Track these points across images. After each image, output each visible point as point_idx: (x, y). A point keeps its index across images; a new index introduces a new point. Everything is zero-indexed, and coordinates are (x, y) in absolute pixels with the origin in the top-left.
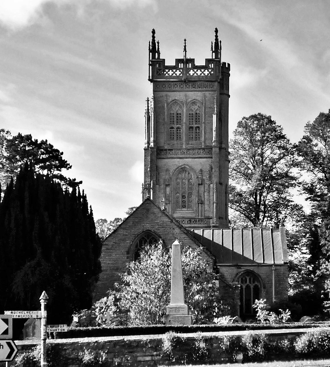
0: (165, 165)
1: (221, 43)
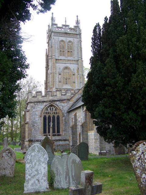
1: (78, 17)
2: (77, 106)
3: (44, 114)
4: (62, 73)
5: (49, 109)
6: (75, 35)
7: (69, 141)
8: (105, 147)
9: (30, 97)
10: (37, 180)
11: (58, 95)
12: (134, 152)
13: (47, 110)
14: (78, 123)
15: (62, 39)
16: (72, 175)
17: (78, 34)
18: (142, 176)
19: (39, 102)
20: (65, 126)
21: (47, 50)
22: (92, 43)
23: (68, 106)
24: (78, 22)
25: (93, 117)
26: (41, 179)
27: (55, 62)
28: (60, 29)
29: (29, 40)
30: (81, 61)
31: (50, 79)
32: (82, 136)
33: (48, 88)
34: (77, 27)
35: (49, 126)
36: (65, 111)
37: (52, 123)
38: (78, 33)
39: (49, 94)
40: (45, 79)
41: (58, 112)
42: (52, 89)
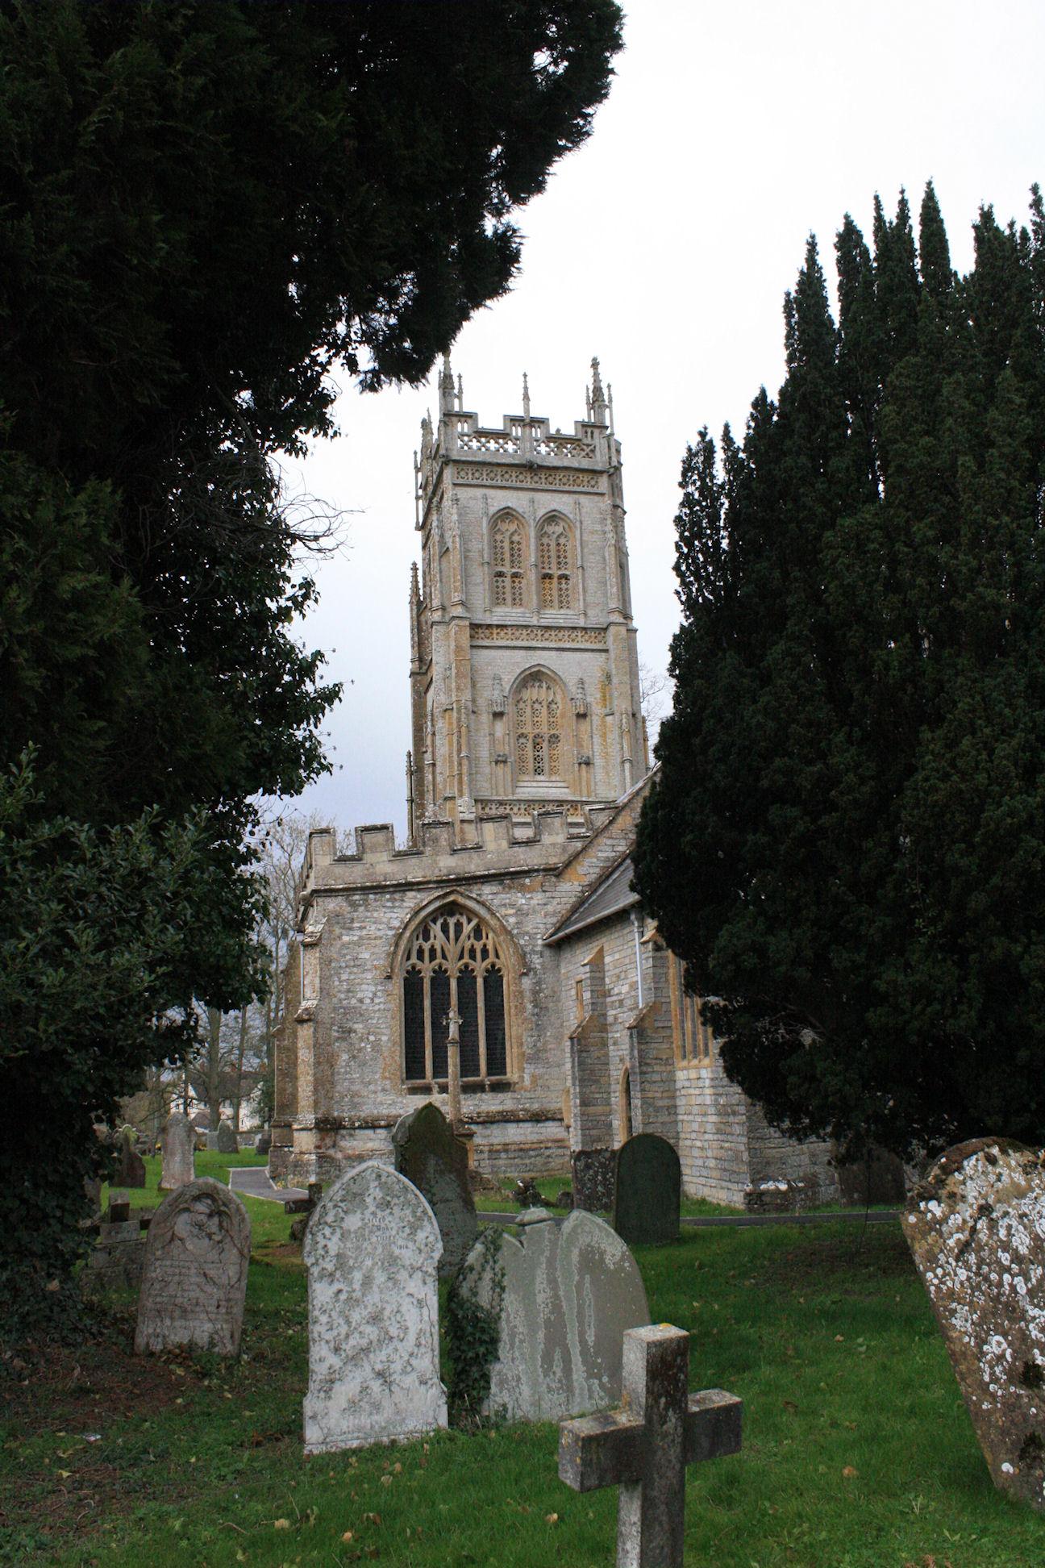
0: (488, 664)
1: (600, 369)
2: (604, 908)
3: (408, 958)
4: (510, 709)
5: (436, 929)
6: (586, 477)
7: (561, 1120)
8: (782, 1161)
9: (323, 861)
10: (380, 1374)
11: (490, 846)
12: (933, 1205)
13: (426, 938)
14: (611, 1012)
15: (516, 499)
16: (583, 1342)
17: (601, 472)
18: (985, 1348)
19: (379, 889)
20: (539, 1028)
21: (415, 569)
22: (678, 547)
23: (550, 908)
24: (597, 399)
25: (694, 983)
26: (404, 1372)
27: (465, 642)
28: (492, 445)
29: (324, 542)
30: (623, 630)
31: (442, 747)
32: (643, 1090)
33: (429, 797)
34: (594, 427)
35: (440, 1031)
36: (532, 937)
37: (452, 1012)
38: (599, 462)
39: (436, 840)
40: (408, 745)
41: (490, 947)
42: (452, 810)
